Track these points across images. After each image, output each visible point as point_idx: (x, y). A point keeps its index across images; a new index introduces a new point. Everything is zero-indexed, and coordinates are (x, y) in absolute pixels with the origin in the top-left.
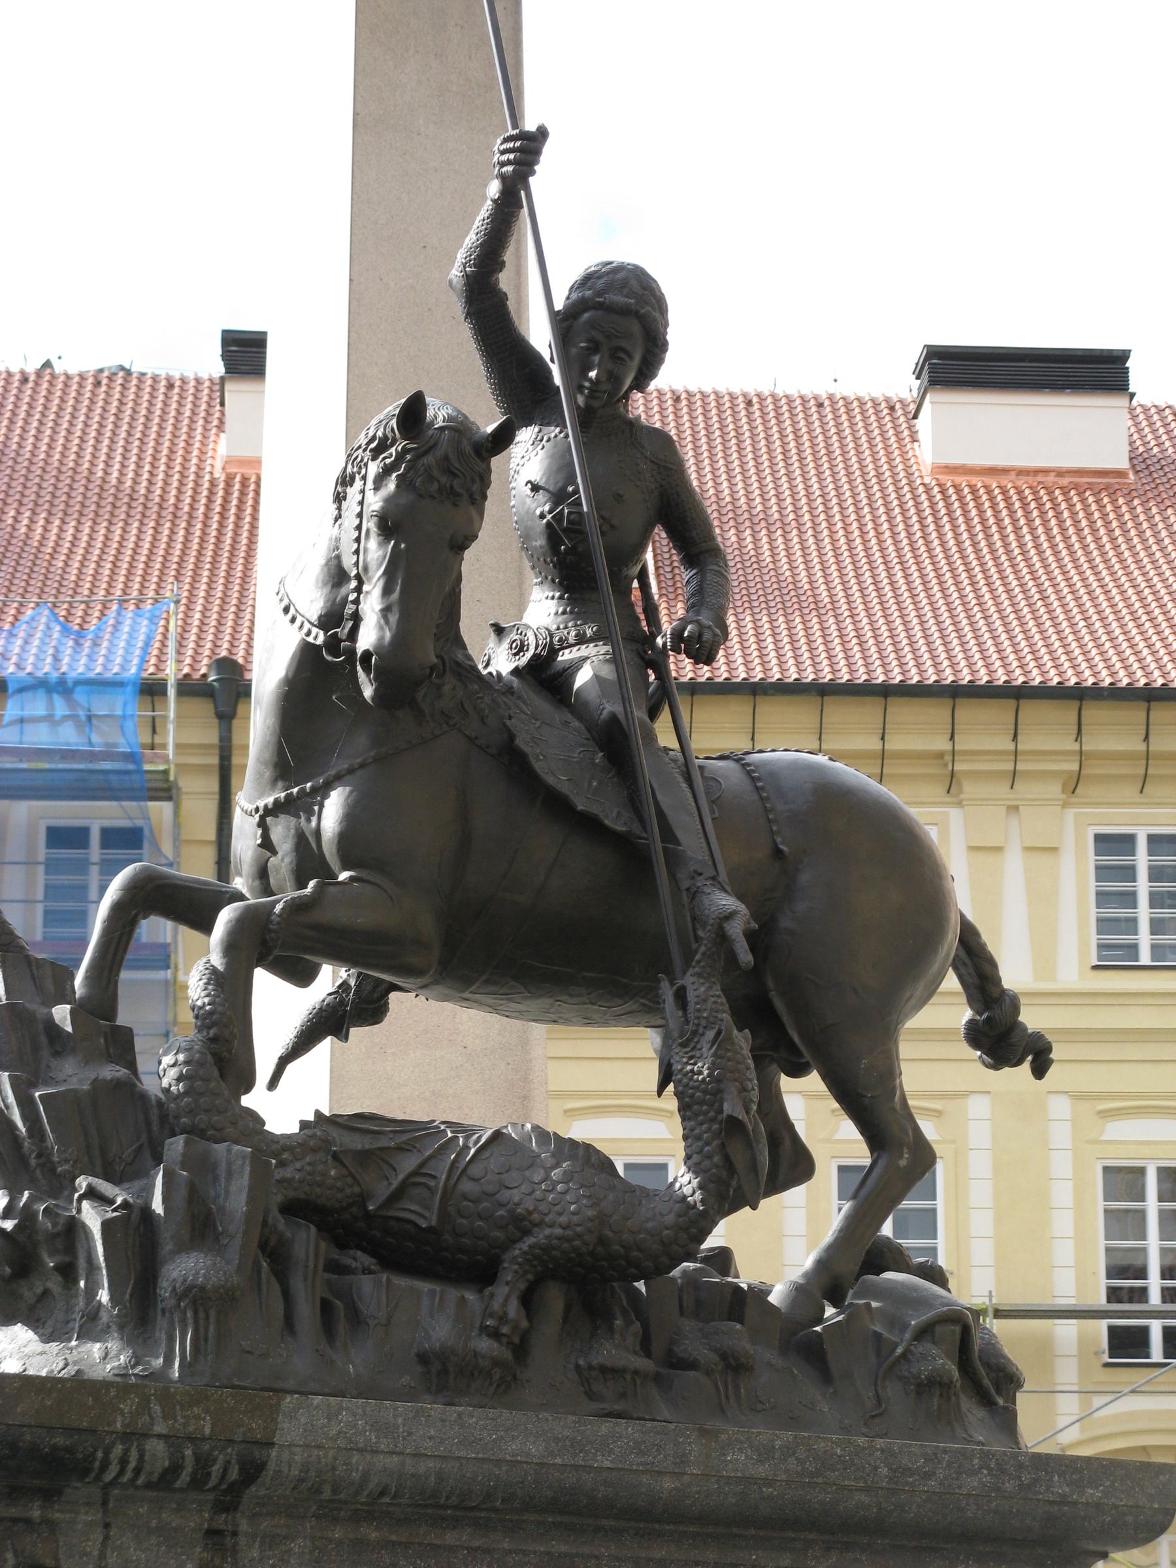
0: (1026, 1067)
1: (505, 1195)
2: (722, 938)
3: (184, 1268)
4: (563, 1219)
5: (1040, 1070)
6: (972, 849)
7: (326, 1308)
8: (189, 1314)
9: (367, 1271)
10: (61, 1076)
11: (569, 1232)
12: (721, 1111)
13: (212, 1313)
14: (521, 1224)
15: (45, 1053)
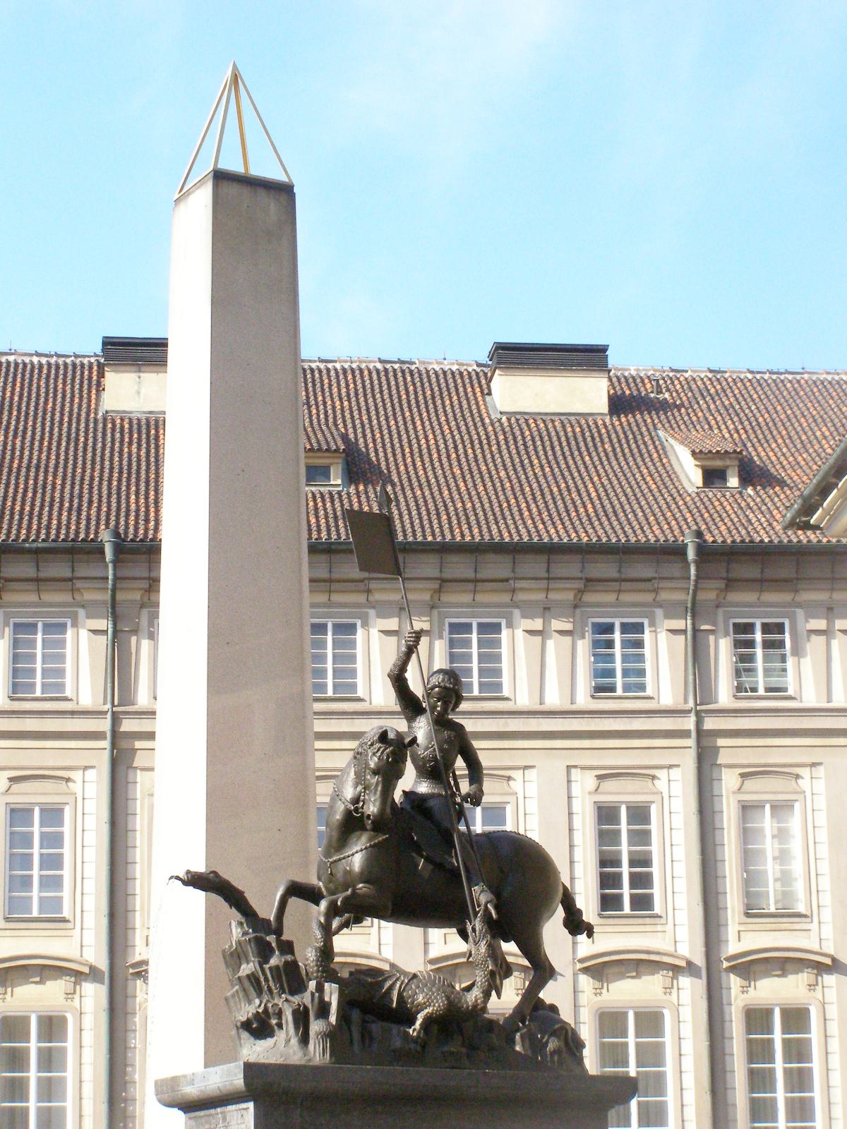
3: (316, 1026)
5: (590, 935)
7: (363, 1037)
9: (374, 1022)
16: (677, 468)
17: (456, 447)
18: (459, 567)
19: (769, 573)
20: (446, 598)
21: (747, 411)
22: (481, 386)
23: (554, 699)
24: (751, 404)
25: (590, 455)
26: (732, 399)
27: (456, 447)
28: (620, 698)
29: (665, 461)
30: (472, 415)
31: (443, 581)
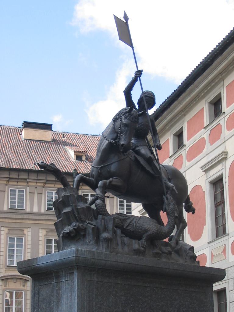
0: (191, 213)
1: (144, 226)
2: (173, 190)
4: (153, 230)
5: (193, 213)
6: (30, 193)
8: (106, 242)
10: (81, 205)
11: (154, 232)
12: (174, 215)
13: (109, 242)
14: (146, 231)
15: (77, 201)
16: (70, 156)
17: (13, 146)
18: (14, 175)
19: (20, 177)
20: (10, 183)
21: (86, 143)
22: (19, 132)
23: (35, 210)
24: (87, 142)
25: (47, 150)
26: (82, 140)
27: (13, 146)
28: (16, 209)
29: (66, 153)
30: (17, 139)
31: (10, 178)
